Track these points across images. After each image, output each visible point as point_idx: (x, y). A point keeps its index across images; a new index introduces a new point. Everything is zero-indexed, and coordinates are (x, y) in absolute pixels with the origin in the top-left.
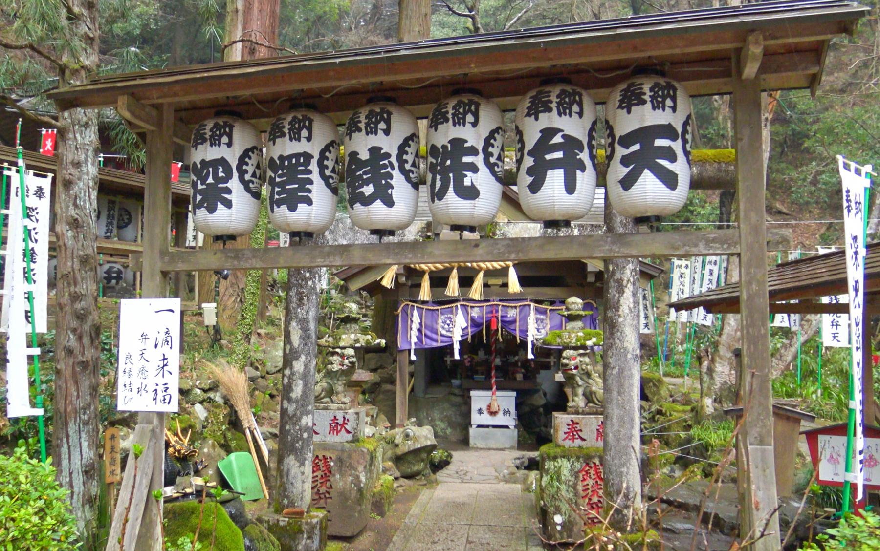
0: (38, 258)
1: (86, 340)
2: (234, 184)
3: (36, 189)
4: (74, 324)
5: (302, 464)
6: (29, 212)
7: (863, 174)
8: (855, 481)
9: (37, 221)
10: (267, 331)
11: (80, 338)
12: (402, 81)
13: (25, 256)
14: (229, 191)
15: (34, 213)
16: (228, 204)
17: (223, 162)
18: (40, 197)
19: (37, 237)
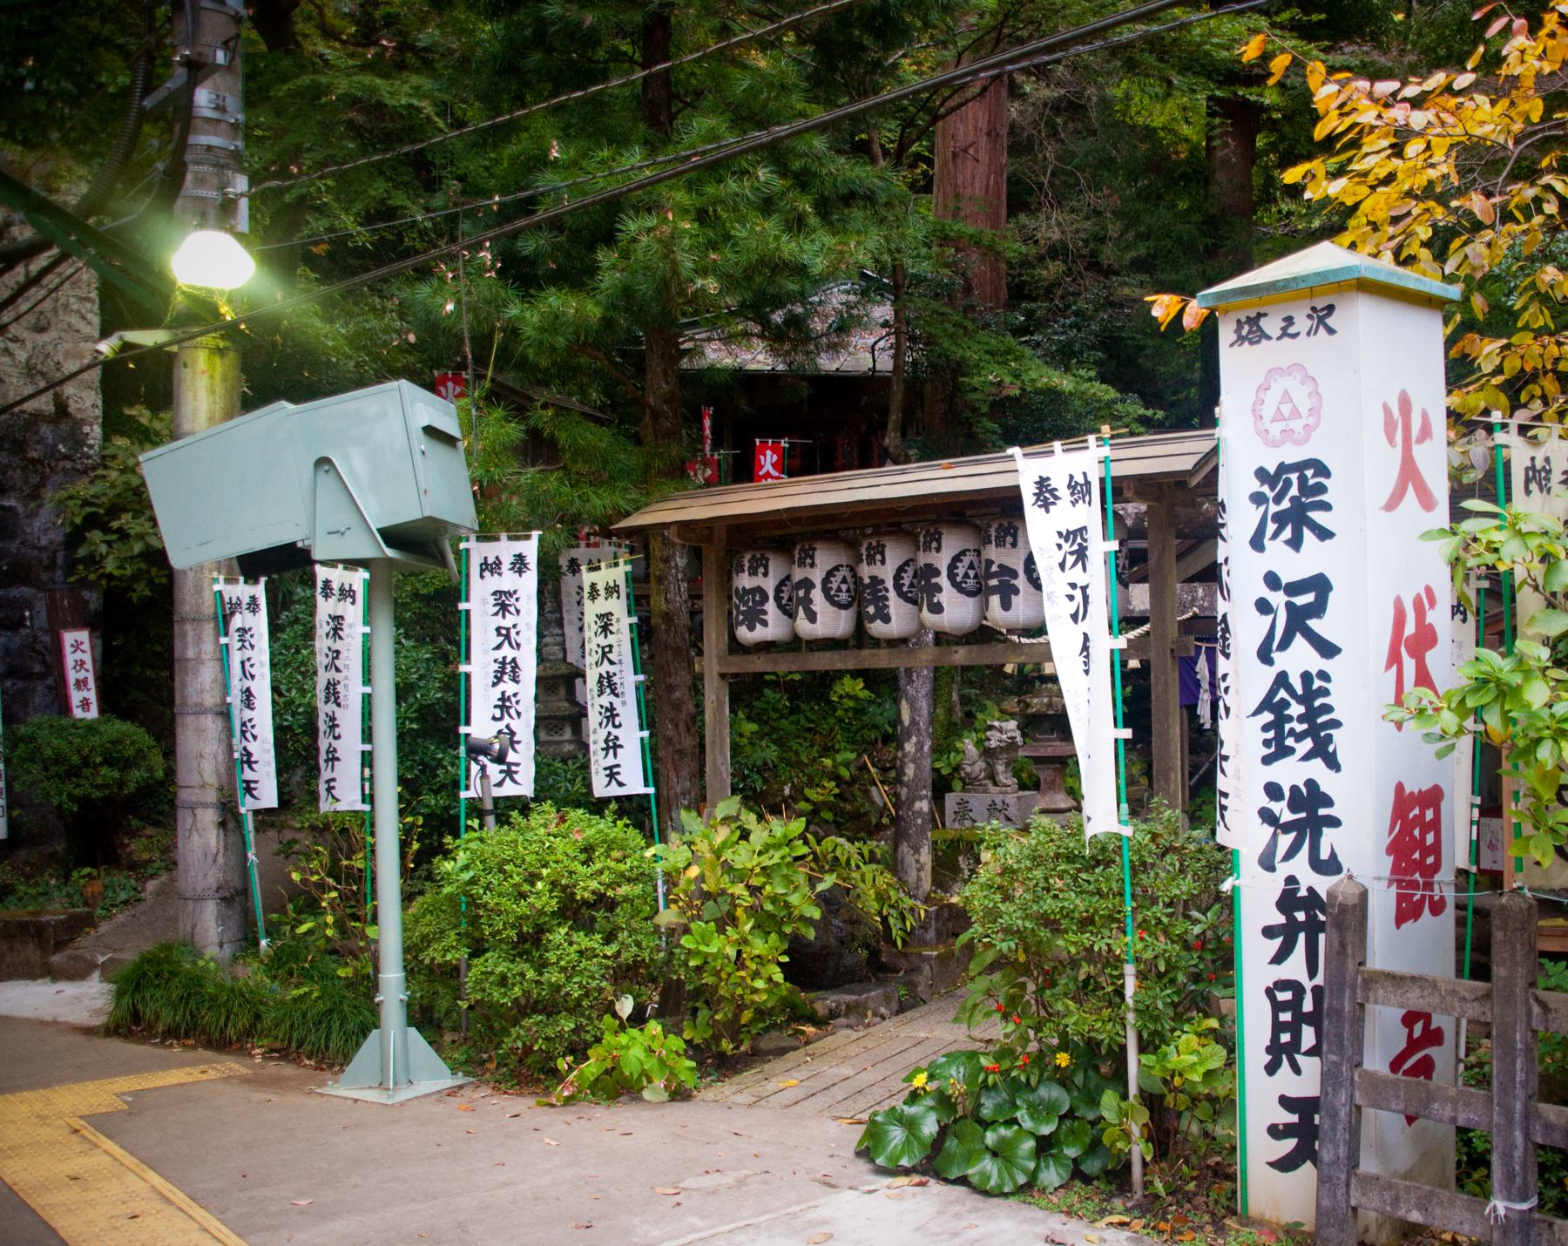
0: (257, 703)
1: (682, 727)
2: (771, 606)
3: (512, 559)
4: (672, 715)
5: (917, 851)
6: (503, 601)
7: (501, 687)
8: (1496, 867)
9: (518, 611)
10: (715, 661)
11: (676, 726)
12: (166, 1066)
13: (1110, 627)
14: (765, 613)
15: (513, 601)
16: (765, 624)
17: (759, 590)
18: (520, 572)
19: (519, 640)
